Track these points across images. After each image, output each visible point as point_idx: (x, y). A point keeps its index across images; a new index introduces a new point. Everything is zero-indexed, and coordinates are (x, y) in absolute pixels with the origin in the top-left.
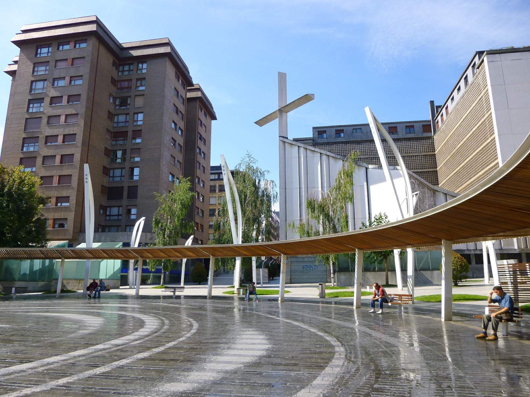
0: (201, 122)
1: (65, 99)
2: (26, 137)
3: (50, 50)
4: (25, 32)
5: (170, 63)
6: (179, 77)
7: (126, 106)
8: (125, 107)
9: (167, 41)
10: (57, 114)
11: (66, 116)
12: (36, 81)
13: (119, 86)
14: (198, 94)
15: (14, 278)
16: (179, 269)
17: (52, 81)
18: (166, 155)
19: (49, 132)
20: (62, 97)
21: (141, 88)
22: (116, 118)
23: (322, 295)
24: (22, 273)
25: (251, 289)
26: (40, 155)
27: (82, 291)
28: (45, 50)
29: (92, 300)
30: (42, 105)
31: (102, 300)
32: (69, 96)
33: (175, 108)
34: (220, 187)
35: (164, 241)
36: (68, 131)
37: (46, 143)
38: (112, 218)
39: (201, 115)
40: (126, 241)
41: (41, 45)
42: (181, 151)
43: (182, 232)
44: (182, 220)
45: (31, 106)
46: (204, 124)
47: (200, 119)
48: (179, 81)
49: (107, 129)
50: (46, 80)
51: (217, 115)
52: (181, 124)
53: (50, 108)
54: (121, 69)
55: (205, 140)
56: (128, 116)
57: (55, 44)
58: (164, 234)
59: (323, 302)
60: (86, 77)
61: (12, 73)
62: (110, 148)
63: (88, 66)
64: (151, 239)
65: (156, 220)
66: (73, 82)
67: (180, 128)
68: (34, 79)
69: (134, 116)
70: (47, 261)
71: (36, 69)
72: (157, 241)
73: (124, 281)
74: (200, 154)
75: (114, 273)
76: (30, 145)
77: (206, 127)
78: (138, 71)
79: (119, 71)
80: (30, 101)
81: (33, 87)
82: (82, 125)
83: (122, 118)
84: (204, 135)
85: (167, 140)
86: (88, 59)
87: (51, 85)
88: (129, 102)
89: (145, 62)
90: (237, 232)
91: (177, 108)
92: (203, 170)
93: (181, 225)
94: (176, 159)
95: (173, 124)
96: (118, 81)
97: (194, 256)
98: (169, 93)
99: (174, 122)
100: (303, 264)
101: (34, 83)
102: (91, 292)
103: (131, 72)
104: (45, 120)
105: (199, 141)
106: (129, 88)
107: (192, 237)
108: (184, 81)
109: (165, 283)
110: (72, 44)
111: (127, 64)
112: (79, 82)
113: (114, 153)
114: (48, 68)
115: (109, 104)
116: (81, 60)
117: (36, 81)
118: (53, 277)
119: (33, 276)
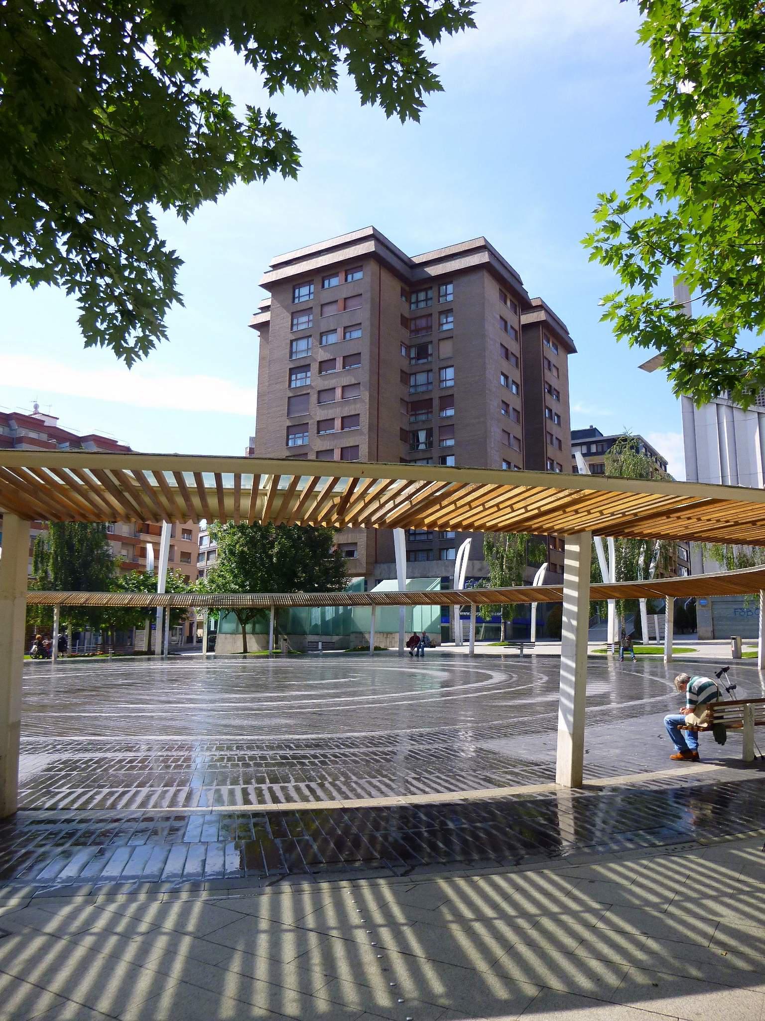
0: (549, 362)
1: (339, 363)
2: (290, 424)
3: (312, 290)
4: (276, 267)
5: (490, 278)
6: (506, 296)
7: (426, 358)
8: (425, 361)
9: (482, 243)
10: (330, 387)
11: (343, 387)
12: (296, 340)
13: (413, 327)
14: (541, 316)
15: (305, 632)
16: (528, 617)
17: (319, 337)
18: (495, 432)
19: (321, 414)
20: (335, 359)
21: (446, 327)
22: (412, 379)
23: (737, 654)
24: (313, 624)
25: (627, 645)
26: (312, 450)
27: (398, 649)
28: (304, 291)
29: (415, 658)
30: (309, 374)
31: (425, 659)
32: (344, 357)
33: (504, 350)
34: (592, 467)
35: (502, 574)
36: (347, 411)
37: (318, 432)
38: (418, 538)
39: (549, 350)
40: (444, 574)
41: (299, 284)
42: (518, 420)
43: (528, 560)
44: (528, 541)
45: (294, 377)
46: (554, 366)
47: (546, 359)
48: (505, 303)
49: (401, 399)
50: (310, 336)
51: (577, 344)
52: (516, 375)
53: (319, 378)
54: (413, 299)
55: (558, 393)
56: (431, 374)
57: (318, 280)
58: (502, 565)
59: (737, 664)
60: (366, 324)
61: (262, 327)
62: (407, 428)
63: (368, 306)
64: (480, 570)
65: (488, 543)
66: (348, 335)
67: (514, 382)
68: (294, 338)
69: (440, 372)
70: (341, 608)
71: (295, 322)
72: (491, 575)
73: (447, 636)
74: (551, 417)
75: (433, 624)
76: (297, 436)
77: (558, 369)
78: (441, 299)
79: (411, 303)
80: (292, 371)
81: (294, 350)
82: (367, 401)
83: (421, 378)
84: (555, 383)
85: (494, 405)
86: (367, 296)
87: (318, 343)
88: (430, 352)
89: (451, 282)
90: (608, 564)
91: (507, 350)
92: (558, 445)
93: (527, 550)
94: (511, 436)
95: (502, 378)
96: (411, 319)
97: (546, 599)
98: (493, 329)
99: (503, 374)
100: (735, 607)
101: (294, 344)
102: (413, 649)
103: (429, 302)
104: (314, 398)
105: (548, 396)
106: (429, 328)
107: (545, 565)
108: (514, 301)
109: (506, 638)
110: (342, 275)
111: (421, 291)
112: (357, 334)
113: (414, 435)
114: (311, 317)
115: (398, 357)
116: (358, 299)
117: (296, 340)
118: (352, 630)
119: (325, 628)
